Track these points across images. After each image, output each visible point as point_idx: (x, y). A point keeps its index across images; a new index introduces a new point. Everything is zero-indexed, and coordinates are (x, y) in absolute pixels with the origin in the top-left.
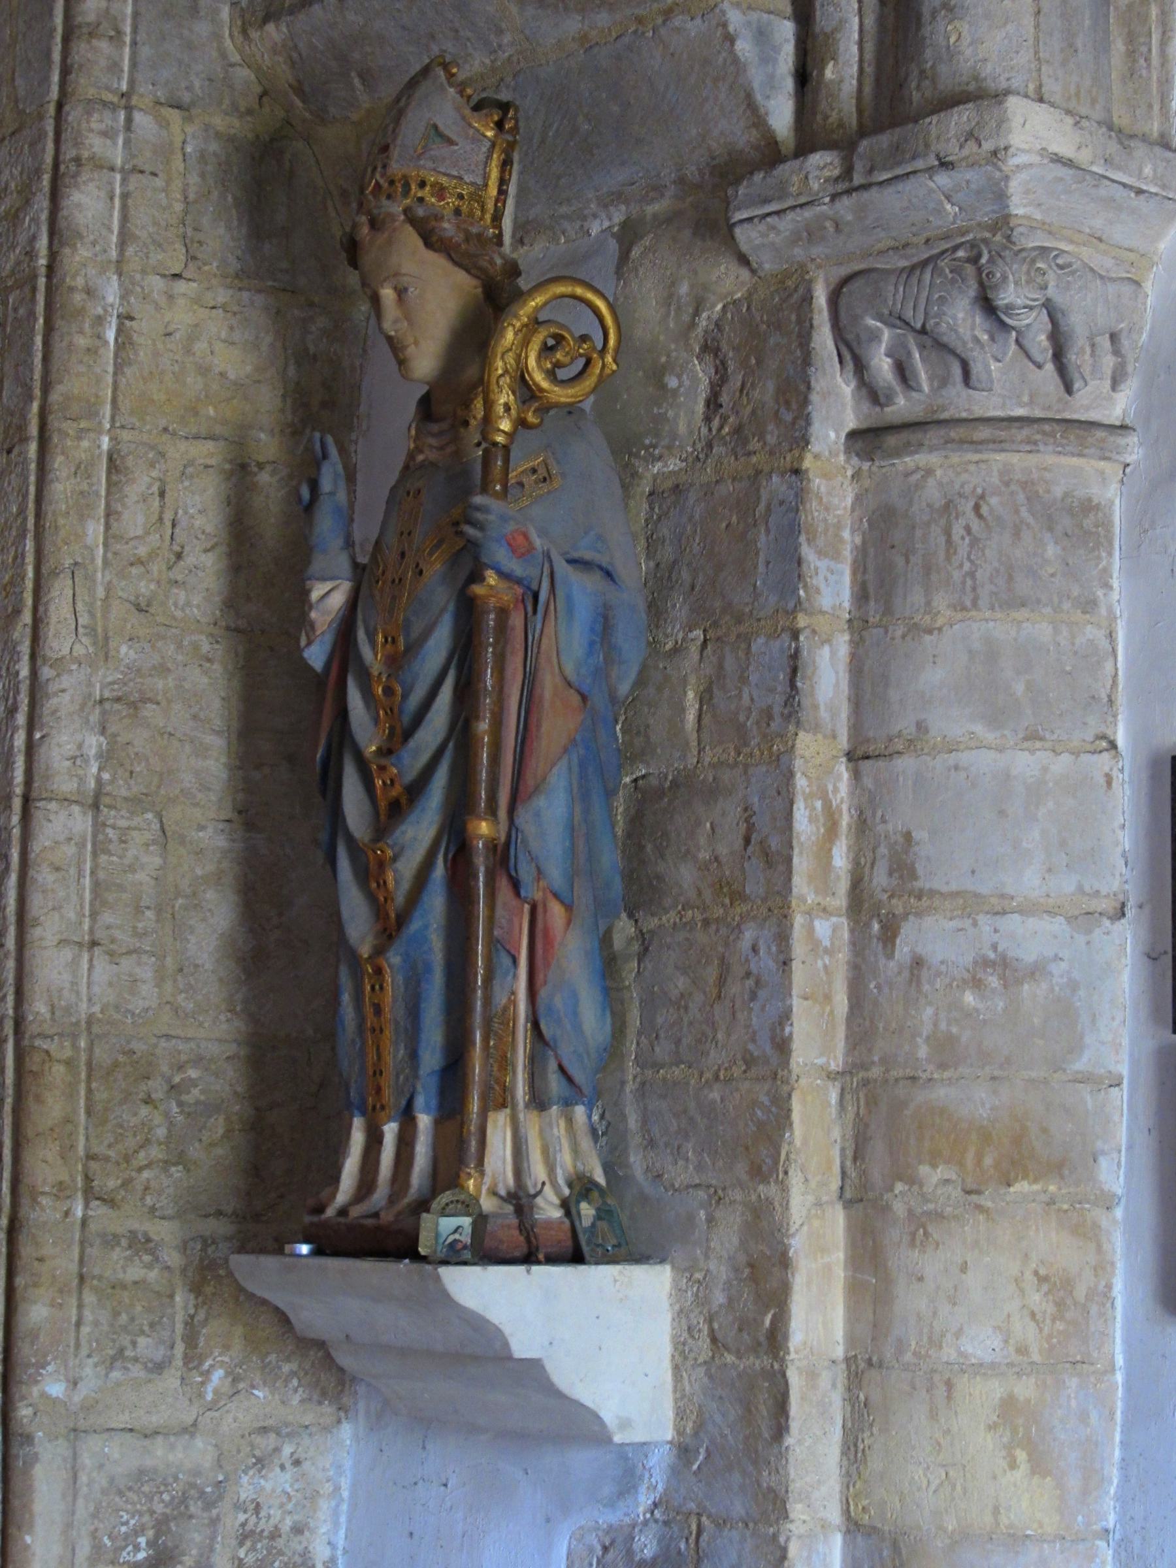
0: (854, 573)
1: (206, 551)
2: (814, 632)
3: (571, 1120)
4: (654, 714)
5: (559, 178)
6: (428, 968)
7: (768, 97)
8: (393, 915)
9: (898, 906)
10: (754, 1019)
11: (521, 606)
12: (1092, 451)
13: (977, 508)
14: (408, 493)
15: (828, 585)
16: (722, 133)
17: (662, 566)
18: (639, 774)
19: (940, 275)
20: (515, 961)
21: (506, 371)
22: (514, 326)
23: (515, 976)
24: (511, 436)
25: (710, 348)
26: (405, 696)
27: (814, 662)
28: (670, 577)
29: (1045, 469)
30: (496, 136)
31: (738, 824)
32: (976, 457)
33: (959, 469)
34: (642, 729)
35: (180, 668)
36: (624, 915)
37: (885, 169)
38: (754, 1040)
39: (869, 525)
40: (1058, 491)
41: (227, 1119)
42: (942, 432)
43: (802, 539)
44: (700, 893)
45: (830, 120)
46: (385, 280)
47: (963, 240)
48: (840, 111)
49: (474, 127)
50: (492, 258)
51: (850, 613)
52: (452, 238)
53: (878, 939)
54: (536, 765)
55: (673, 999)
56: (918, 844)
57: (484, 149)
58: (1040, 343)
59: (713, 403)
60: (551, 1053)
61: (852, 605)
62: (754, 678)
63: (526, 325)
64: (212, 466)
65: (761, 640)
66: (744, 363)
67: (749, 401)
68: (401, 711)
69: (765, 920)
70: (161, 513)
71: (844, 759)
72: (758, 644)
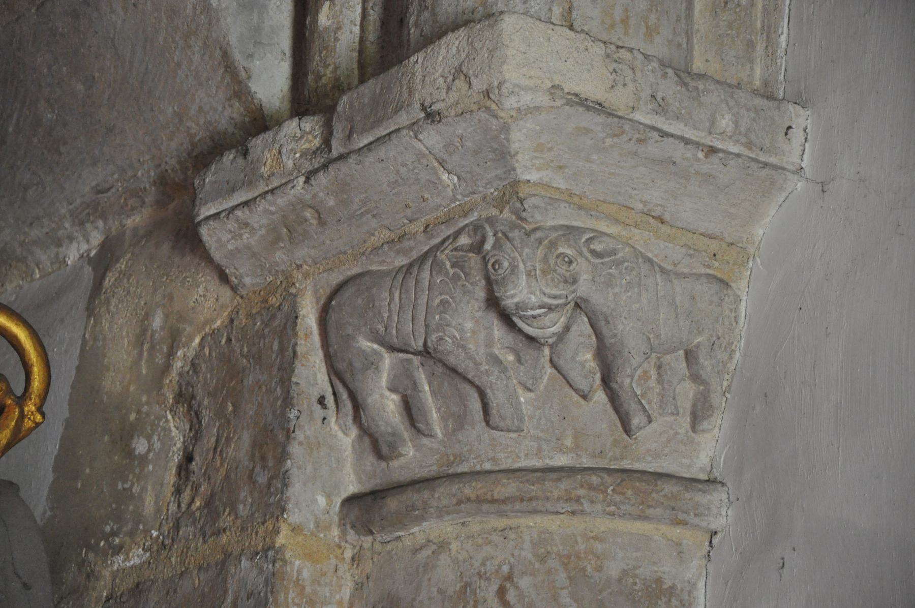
5: (26, 189)
7: (251, 56)
12: (659, 511)
13: (501, 592)
16: (201, 109)
19: (439, 272)
25: (185, 397)
29: (596, 538)
32: (503, 523)
33: (480, 541)
37: (364, 131)
40: (613, 569)
42: (455, 488)
45: (324, 81)
47: (466, 222)
48: (336, 68)
58: (583, 365)
66: (220, 413)
67: (223, 460)
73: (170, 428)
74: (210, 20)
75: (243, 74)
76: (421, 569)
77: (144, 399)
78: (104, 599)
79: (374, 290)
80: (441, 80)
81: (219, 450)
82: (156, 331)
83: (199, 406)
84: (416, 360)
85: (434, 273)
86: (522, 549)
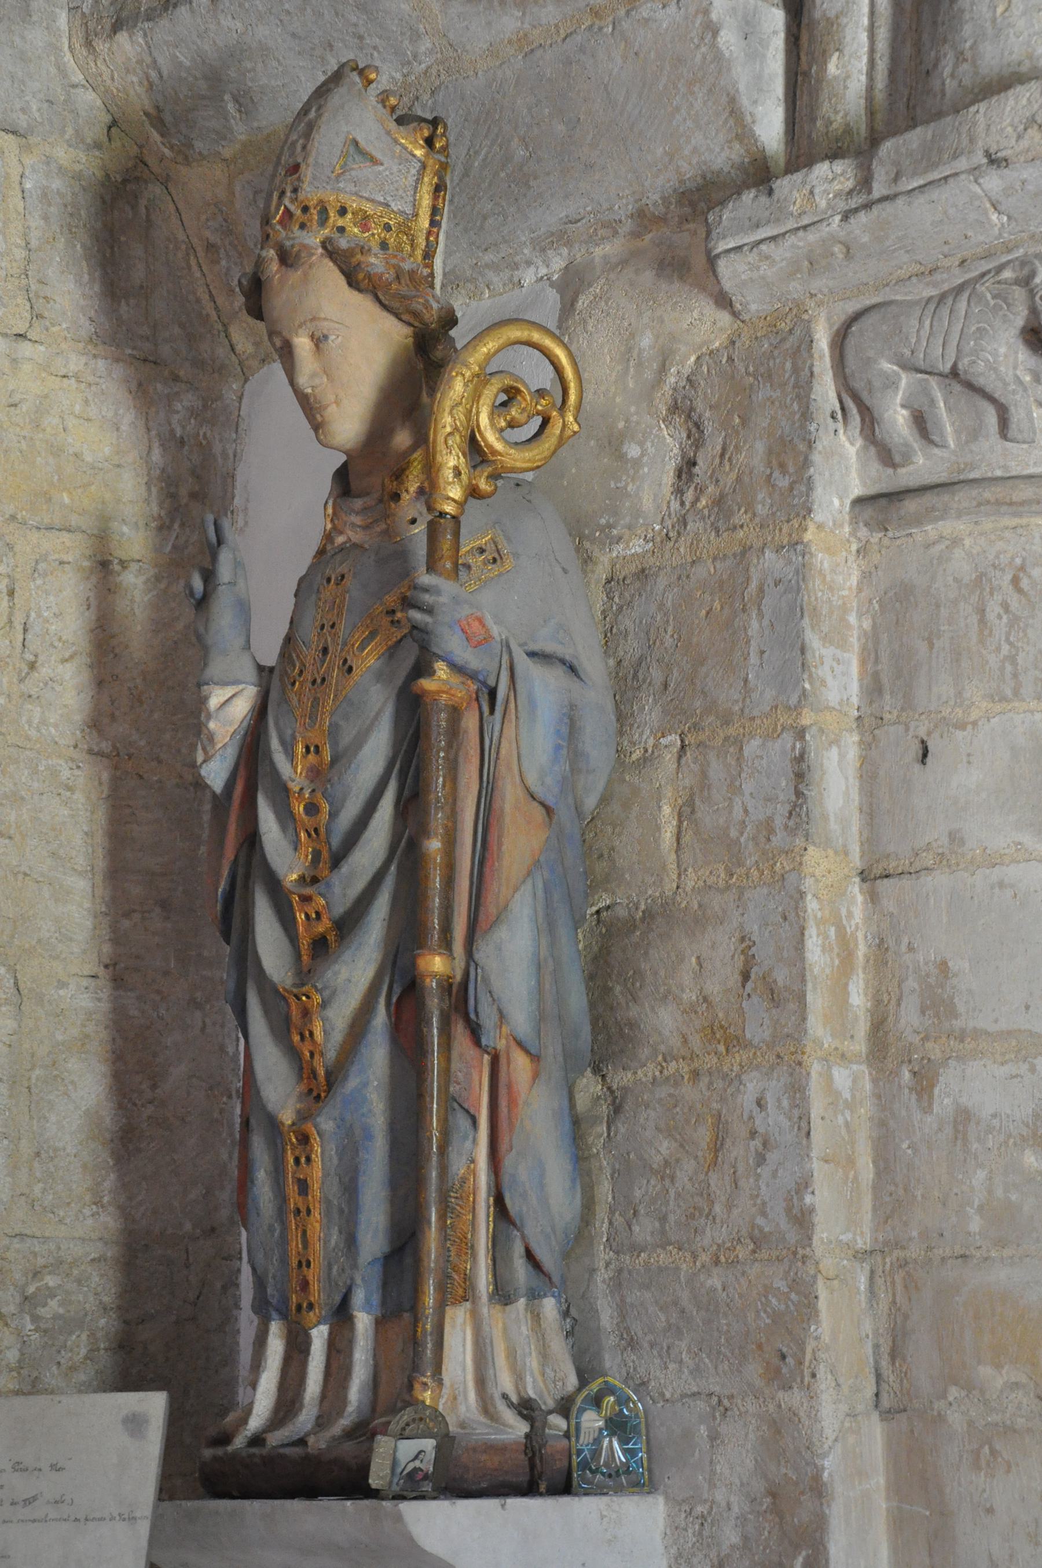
0: (863, 662)
1: (64, 661)
2: (821, 731)
3: (538, 1315)
4: (620, 835)
5: (485, 218)
6: (369, 1136)
7: (755, 102)
8: (321, 1072)
9: (934, 1050)
10: (763, 1187)
11: (475, 705)
13: (1015, 581)
14: (329, 580)
15: (834, 677)
16: (695, 150)
17: (625, 664)
18: (601, 905)
20: (474, 1121)
21: (456, 429)
22: (463, 375)
23: (475, 1141)
24: (461, 504)
26: (333, 815)
27: (822, 765)
28: (636, 673)
30: (427, 155)
31: (733, 956)
32: (1015, 521)
33: (993, 537)
34: (606, 853)
35: (36, 797)
36: (588, 1072)
37: (914, 174)
38: (764, 1214)
39: (881, 606)
41: (92, 1335)
42: (974, 493)
43: (806, 622)
44: (685, 1041)
45: (835, 126)
46: (300, 326)
47: (1010, 258)
48: (846, 115)
49: (400, 144)
50: (427, 301)
51: (858, 710)
52: (382, 274)
53: (911, 1089)
54: (497, 890)
55: (655, 1166)
56: (955, 975)
57: (414, 171)
59: (686, 468)
60: (515, 1232)
61: (861, 699)
62: (748, 787)
63: (478, 376)
64: (69, 563)
65: (756, 743)
68: (328, 831)
69: (772, 1068)
70: (11, 615)
71: (857, 880)
72: (752, 747)
73: (664, 437)
74: (720, 69)
75: (749, 118)
76: (935, 562)
77: (633, 409)
78: (604, 582)
79: (902, 318)
80: (1010, 129)
81: (727, 456)
82: (644, 350)
83: (700, 418)
84: (933, 382)
85: (972, 304)
86: (1032, 544)
